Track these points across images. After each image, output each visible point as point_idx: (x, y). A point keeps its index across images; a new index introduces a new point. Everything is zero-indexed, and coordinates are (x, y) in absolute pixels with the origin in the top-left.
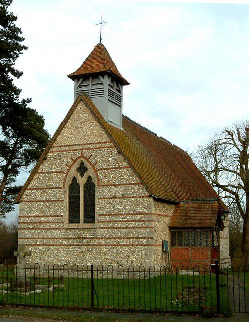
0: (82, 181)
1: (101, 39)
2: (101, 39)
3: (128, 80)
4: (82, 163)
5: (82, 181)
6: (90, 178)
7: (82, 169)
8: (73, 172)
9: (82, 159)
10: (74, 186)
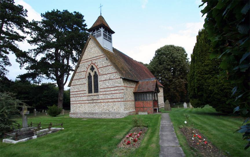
0: (92, 74)
1: (101, 14)
2: (101, 14)
3: (115, 32)
4: (92, 66)
7: (92, 69)
8: (89, 71)
10: (90, 77)
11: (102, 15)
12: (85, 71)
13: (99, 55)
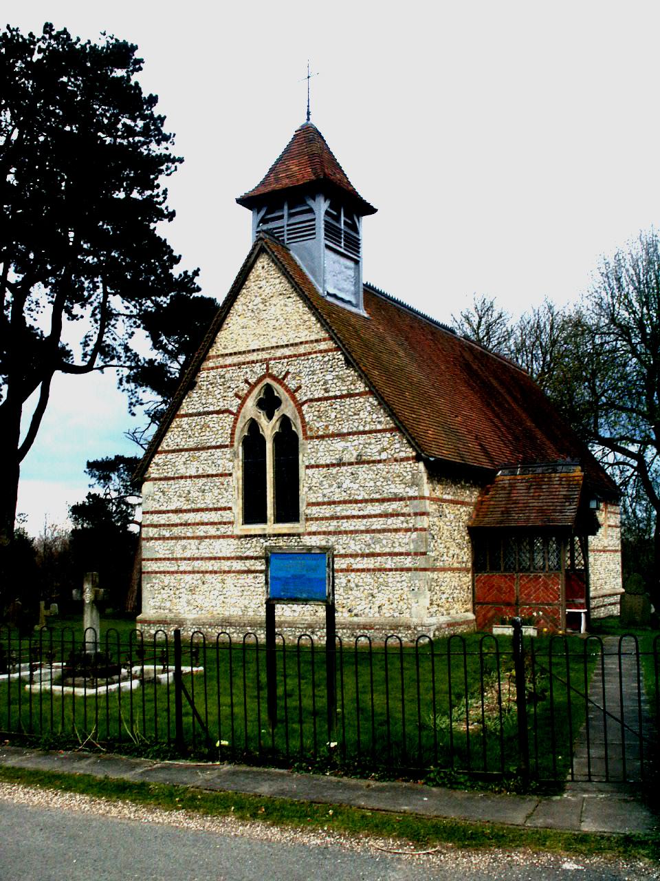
0: (269, 428)
1: (308, 113)
2: (308, 113)
4: (269, 389)
5: (269, 428)
6: (285, 421)
7: (269, 403)
9: (268, 380)
10: (253, 442)
11: (314, 121)
12: (231, 413)
13: (304, 335)
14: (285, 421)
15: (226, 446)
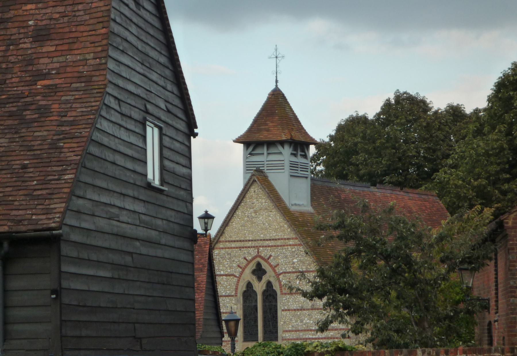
1: (277, 81)
2: (277, 81)
4: (259, 265)
6: (269, 284)
8: (248, 276)
9: (259, 259)
11: (280, 87)
13: (280, 235)
14: (269, 284)
15: (233, 296)
